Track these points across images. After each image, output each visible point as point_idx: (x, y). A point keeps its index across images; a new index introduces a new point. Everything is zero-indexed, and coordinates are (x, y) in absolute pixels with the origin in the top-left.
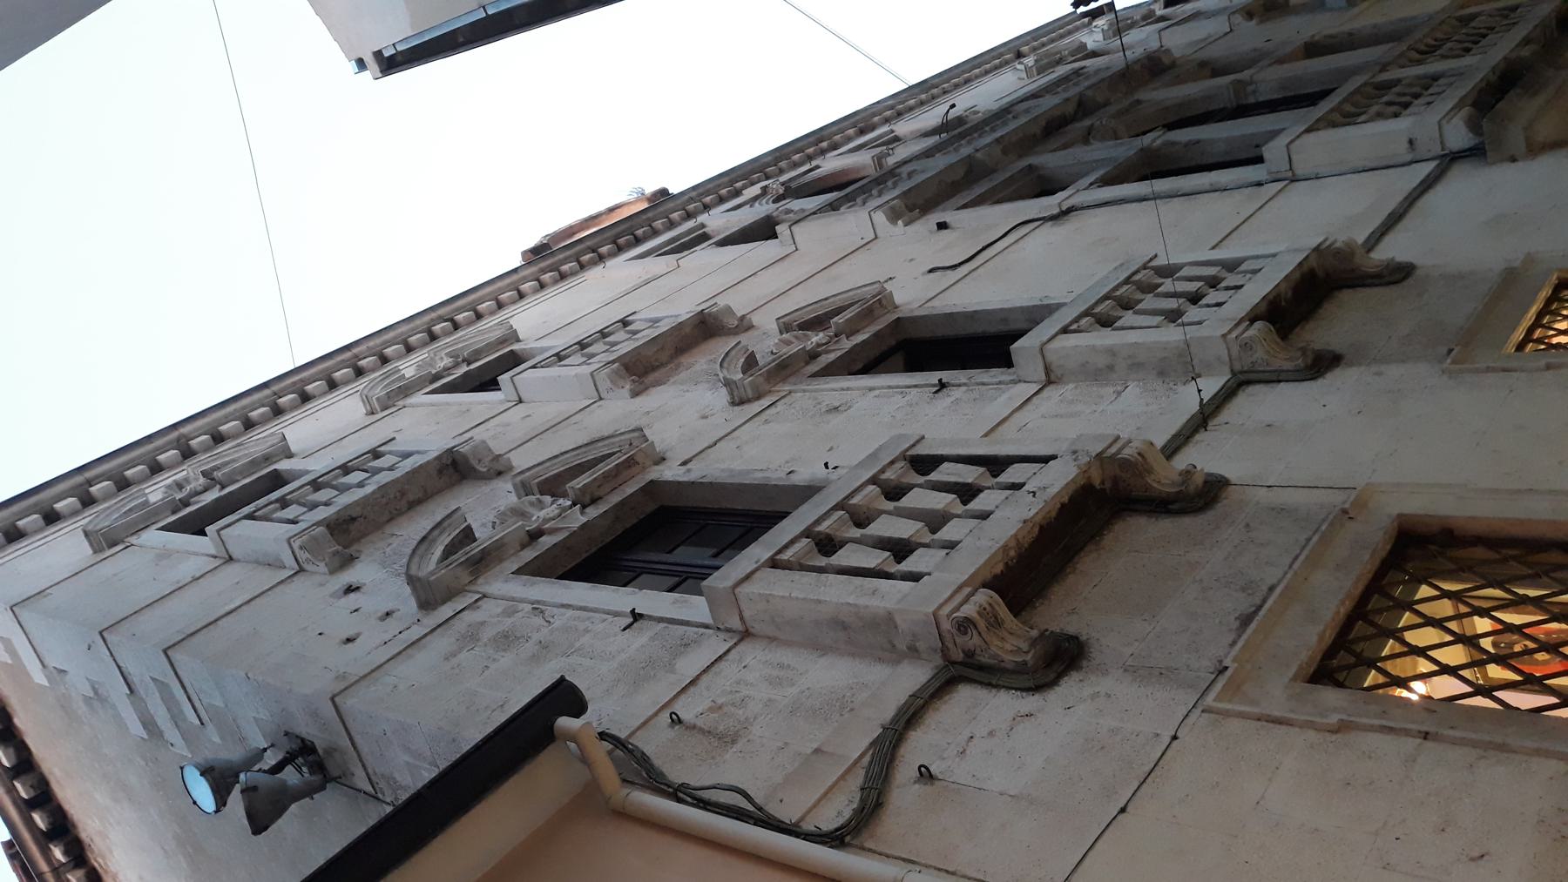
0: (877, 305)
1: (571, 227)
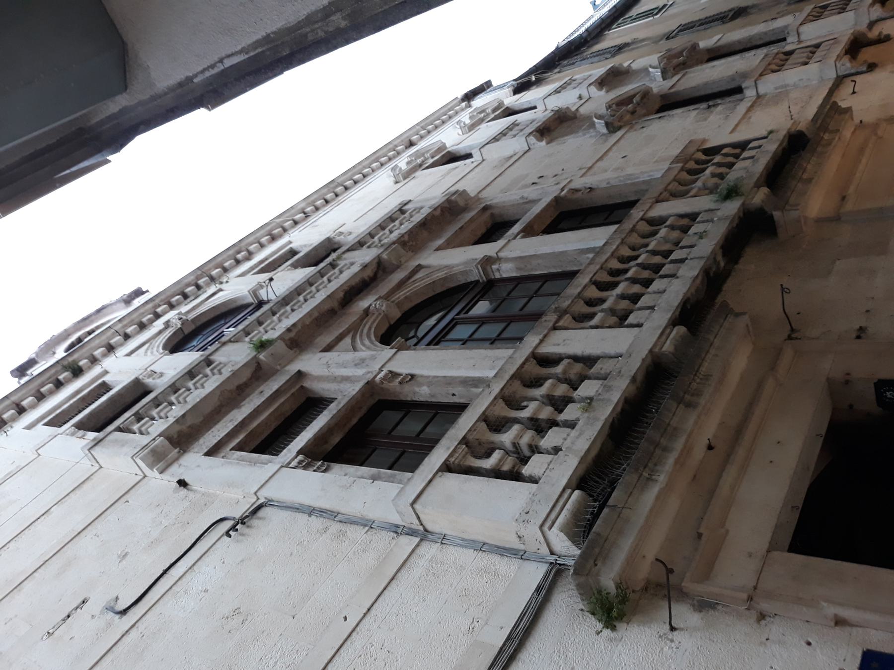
1: (66, 331)
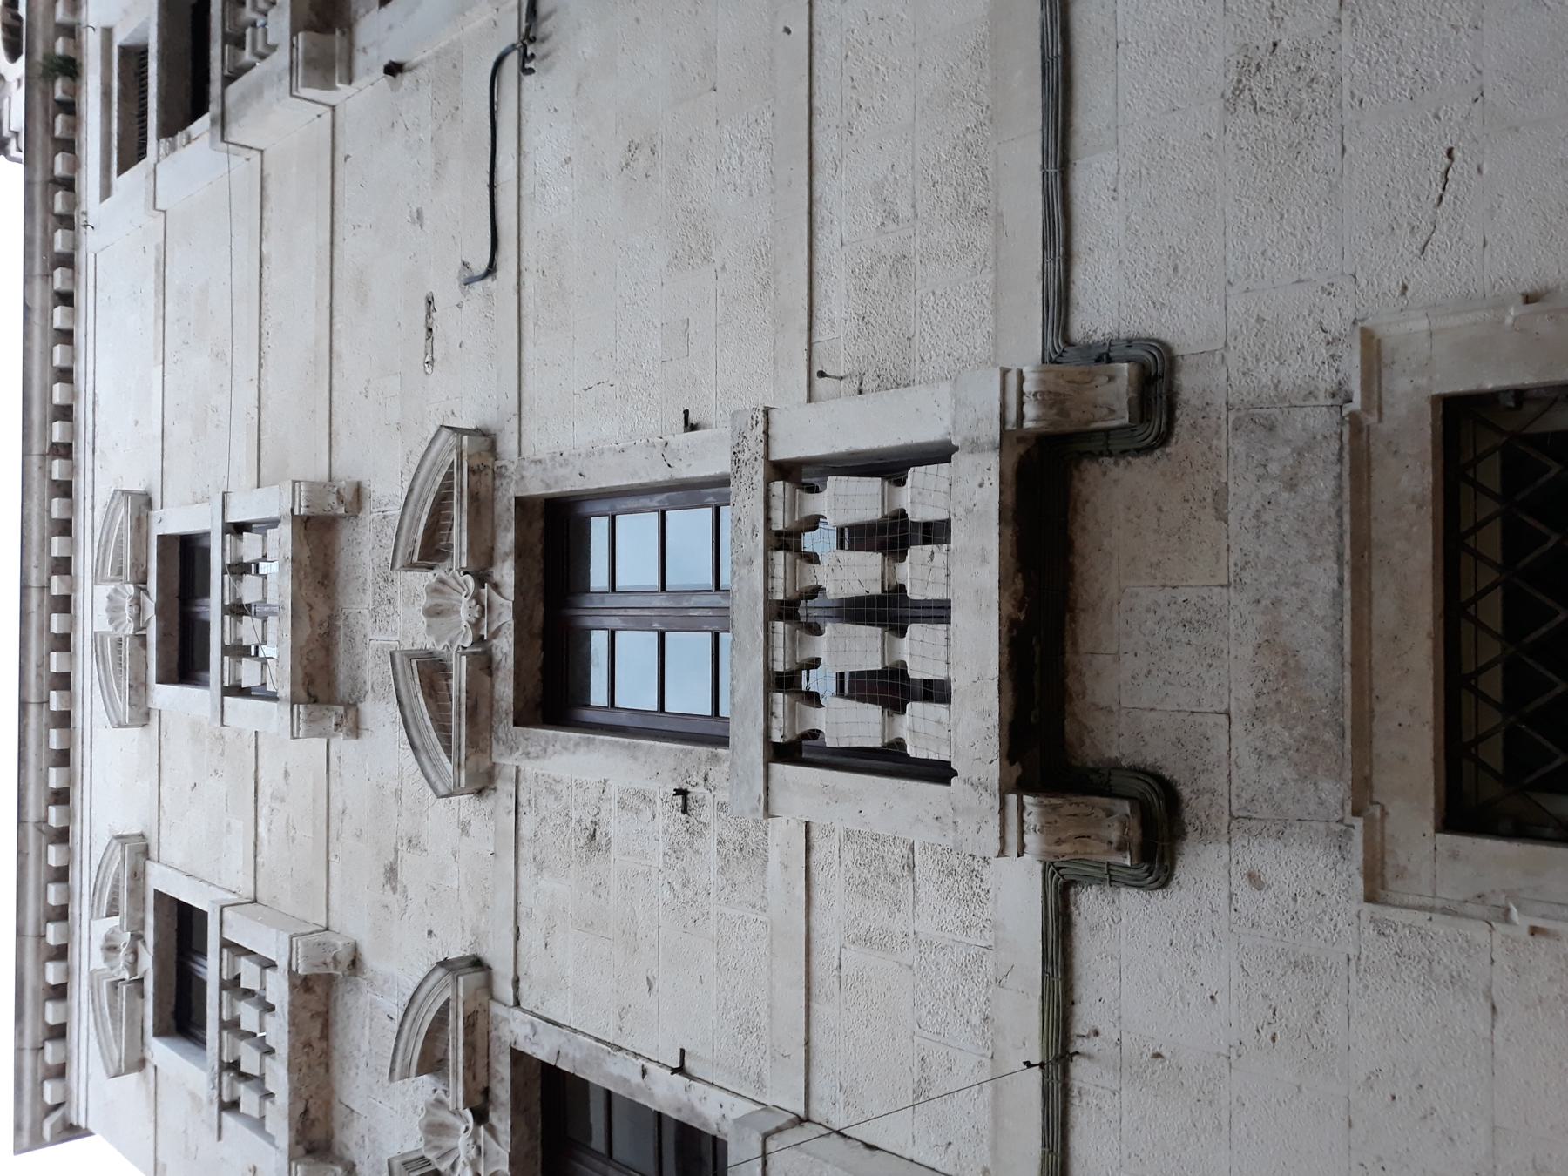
0: (474, 478)
